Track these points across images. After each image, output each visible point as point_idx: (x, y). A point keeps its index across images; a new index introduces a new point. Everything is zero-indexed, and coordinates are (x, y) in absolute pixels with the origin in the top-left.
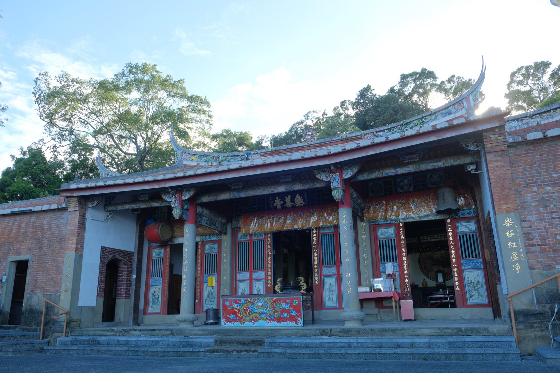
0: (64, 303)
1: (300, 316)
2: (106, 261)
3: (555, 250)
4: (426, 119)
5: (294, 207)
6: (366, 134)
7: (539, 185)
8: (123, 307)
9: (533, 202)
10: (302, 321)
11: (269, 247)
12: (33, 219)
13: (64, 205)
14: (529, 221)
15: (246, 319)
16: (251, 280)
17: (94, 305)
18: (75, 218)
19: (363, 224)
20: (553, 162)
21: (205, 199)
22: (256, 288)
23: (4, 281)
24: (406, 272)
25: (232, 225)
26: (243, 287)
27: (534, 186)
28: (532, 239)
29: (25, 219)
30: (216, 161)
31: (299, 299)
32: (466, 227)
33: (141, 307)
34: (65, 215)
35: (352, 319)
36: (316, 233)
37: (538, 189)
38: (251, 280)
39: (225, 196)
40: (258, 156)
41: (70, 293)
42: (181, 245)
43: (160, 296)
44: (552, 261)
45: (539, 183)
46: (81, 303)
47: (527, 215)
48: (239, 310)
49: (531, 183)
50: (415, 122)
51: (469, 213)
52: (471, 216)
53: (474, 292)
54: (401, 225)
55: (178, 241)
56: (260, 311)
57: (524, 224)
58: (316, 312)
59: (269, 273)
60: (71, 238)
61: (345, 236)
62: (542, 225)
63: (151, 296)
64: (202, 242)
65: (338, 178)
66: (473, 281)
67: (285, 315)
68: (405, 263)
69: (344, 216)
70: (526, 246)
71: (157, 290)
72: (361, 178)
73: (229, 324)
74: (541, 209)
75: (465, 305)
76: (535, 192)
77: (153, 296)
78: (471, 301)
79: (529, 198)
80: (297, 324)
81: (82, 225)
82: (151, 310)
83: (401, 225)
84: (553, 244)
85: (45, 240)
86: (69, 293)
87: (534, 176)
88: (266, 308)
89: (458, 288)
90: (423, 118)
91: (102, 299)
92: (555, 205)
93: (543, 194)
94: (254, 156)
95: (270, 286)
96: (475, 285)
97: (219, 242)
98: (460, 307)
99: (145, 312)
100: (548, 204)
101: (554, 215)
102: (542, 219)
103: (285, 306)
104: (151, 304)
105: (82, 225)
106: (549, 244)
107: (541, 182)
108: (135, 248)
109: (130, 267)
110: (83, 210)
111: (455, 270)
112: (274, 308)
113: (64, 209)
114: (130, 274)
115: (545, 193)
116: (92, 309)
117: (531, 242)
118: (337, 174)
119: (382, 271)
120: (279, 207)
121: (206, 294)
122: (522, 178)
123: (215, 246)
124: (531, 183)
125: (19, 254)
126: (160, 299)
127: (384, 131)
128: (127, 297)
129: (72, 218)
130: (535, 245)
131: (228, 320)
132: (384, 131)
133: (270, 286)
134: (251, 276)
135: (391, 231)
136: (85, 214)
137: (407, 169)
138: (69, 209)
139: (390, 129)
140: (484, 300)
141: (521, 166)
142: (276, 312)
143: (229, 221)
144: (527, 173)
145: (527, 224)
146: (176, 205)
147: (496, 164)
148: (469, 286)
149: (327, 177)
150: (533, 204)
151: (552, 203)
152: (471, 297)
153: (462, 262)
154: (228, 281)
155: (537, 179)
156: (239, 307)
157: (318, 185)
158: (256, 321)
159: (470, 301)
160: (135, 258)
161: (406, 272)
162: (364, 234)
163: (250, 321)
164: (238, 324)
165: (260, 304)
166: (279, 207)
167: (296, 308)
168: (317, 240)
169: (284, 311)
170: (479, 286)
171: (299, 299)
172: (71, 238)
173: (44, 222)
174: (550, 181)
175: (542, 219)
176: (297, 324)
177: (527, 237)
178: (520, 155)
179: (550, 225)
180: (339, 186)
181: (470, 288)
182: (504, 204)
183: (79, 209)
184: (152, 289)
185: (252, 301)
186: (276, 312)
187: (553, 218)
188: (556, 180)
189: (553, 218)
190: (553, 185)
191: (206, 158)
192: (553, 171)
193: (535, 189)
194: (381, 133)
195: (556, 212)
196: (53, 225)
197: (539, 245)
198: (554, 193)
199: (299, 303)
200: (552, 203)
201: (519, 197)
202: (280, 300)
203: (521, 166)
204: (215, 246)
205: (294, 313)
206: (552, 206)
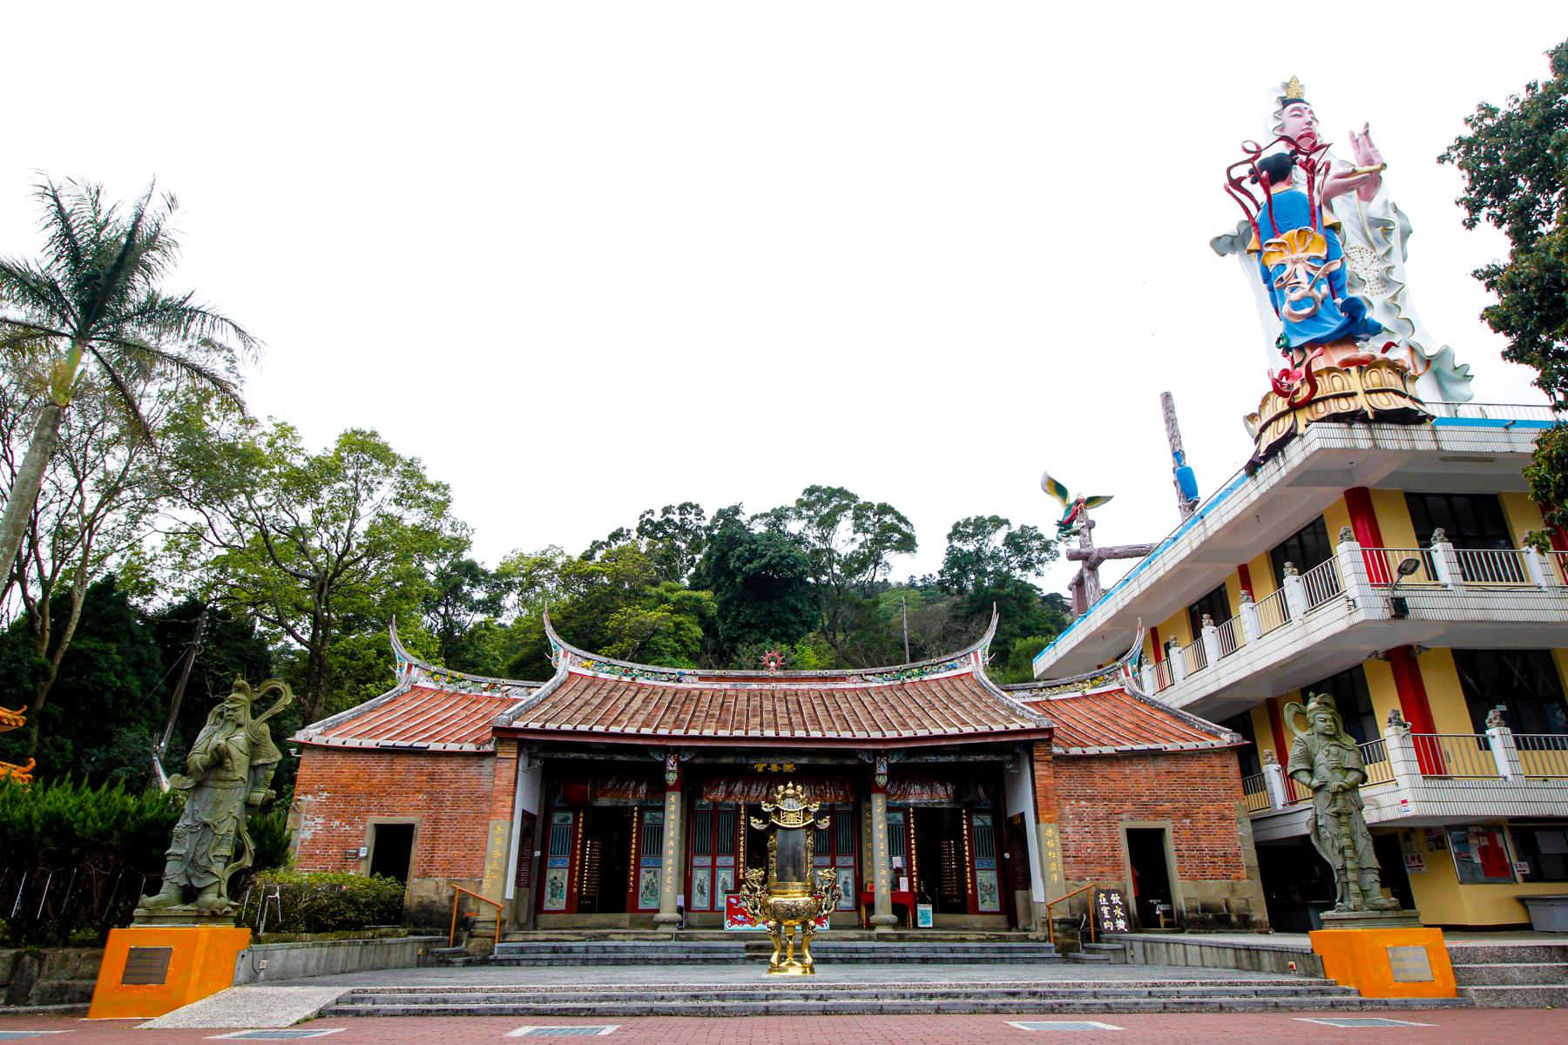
12: (426, 765)
13: (489, 748)
16: (713, 868)
23: (362, 855)
29: (402, 764)
35: (887, 924)
38: (713, 868)
40: (695, 679)
63: (548, 884)
73: (736, 927)
82: (548, 906)
94: (689, 679)
104: (548, 896)
121: (643, 884)
125: (393, 813)
131: (734, 921)
134: (714, 861)
140: (996, 907)
159: (982, 908)
164: (747, 926)
184: (551, 874)
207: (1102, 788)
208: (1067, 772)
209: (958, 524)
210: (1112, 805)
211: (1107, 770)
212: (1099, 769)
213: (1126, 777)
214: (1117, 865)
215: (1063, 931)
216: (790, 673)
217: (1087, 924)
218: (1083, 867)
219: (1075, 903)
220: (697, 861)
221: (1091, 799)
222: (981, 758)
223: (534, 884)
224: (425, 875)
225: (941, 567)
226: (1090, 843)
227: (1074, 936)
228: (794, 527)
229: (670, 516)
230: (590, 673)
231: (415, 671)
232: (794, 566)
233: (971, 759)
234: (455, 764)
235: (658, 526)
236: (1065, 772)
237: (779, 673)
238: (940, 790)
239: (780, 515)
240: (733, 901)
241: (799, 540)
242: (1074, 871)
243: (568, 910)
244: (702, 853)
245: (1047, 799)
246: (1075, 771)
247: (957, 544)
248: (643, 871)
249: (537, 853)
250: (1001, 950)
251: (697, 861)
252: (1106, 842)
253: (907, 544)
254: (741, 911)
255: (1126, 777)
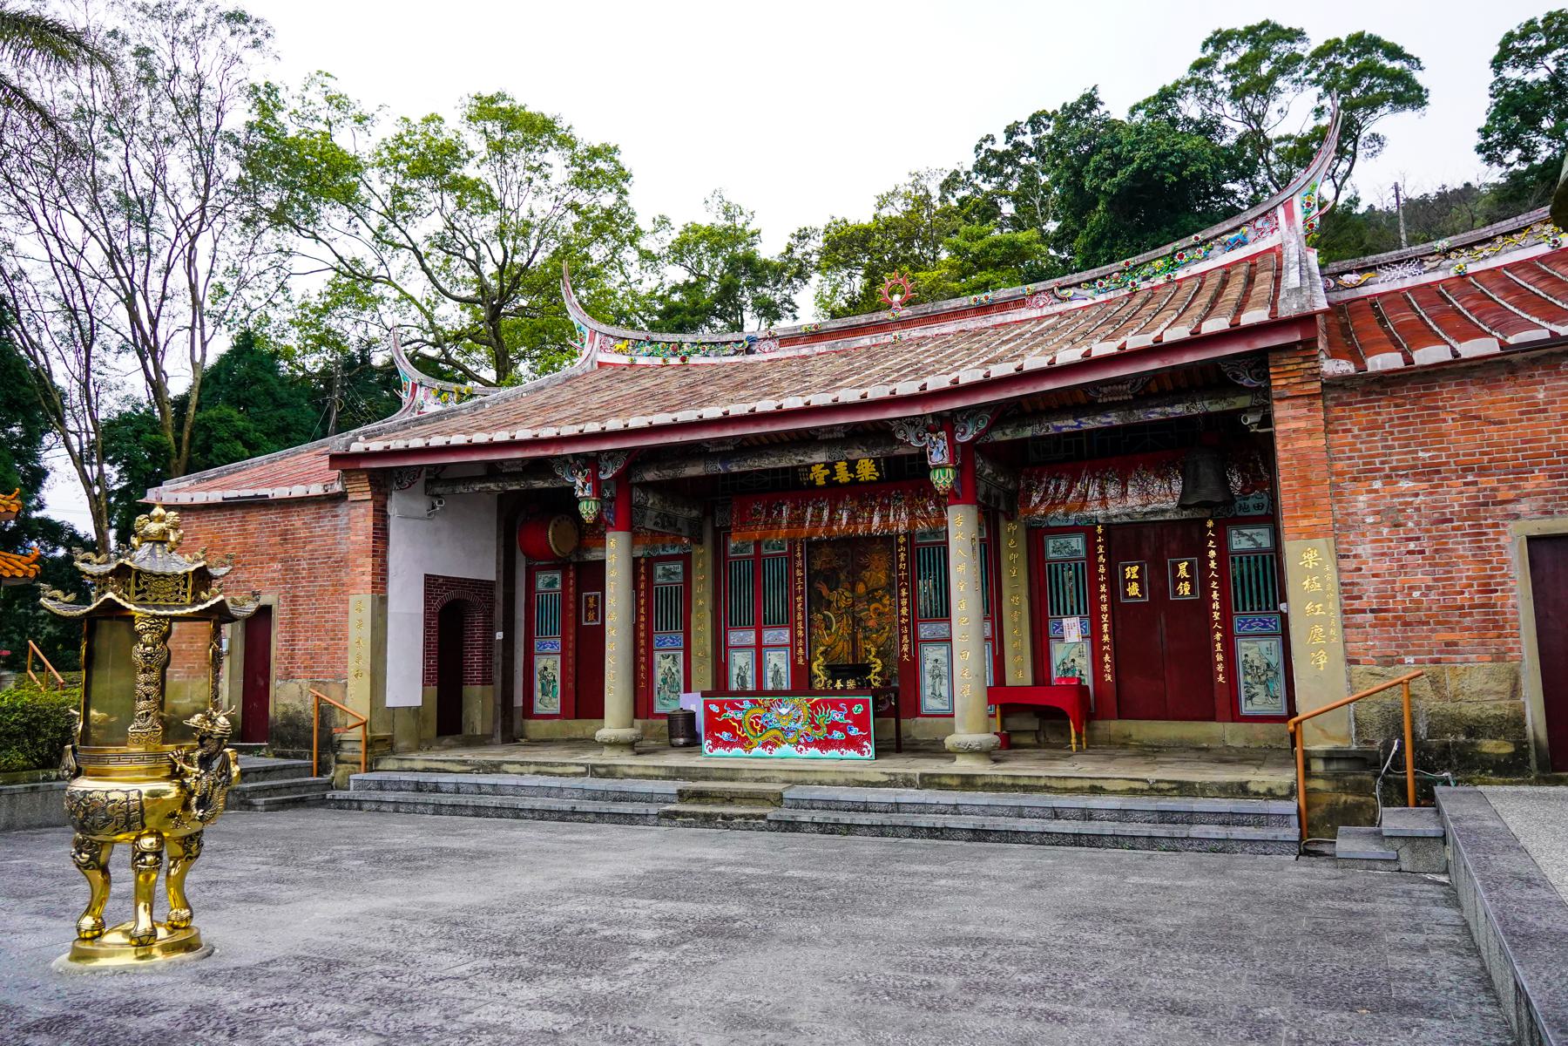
0: (356, 702)
1: (868, 738)
2: (436, 606)
3: (1406, 624)
4: (1181, 257)
5: (855, 481)
6: (1035, 293)
7: (1389, 476)
8: (479, 704)
9: (1369, 514)
10: (872, 749)
11: (799, 573)
13: (338, 488)
14: (1355, 556)
15: (756, 741)
16: (759, 648)
17: (417, 701)
18: (364, 516)
19: (1012, 527)
20: (1422, 423)
21: (650, 476)
22: (771, 665)
24: (1106, 638)
25: (713, 522)
26: (741, 662)
27: (1375, 479)
28: (1360, 598)
29: (256, 520)
30: (674, 356)
31: (865, 703)
32: (1250, 538)
33: (519, 701)
34: (342, 510)
35: (970, 751)
36: (905, 544)
37: (1384, 484)
38: (759, 648)
39: (692, 471)
41: (368, 680)
42: (601, 564)
43: (558, 678)
44: (1398, 646)
45: (1387, 471)
46: (390, 702)
47: (1353, 543)
48: (739, 722)
49: (1370, 471)
50: (1156, 264)
51: (1258, 507)
52: (1262, 512)
53: (1259, 689)
54: (1100, 530)
55: (593, 556)
56: (782, 724)
57: (1345, 564)
58: (905, 723)
59: (800, 633)
60: (359, 562)
61: (960, 569)
62: (1386, 564)
63: (537, 676)
64: (648, 559)
65: (942, 445)
66: (1257, 663)
67: (837, 735)
68: (1105, 618)
69: (961, 526)
70: (1345, 612)
71: (550, 663)
72: (998, 436)
73: (719, 751)
74: (1385, 531)
75: (1236, 716)
76: (1376, 491)
77: (544, 677)
78: (1249, 707)
79: (1361, 505)
80: (863, 753)
81: (381, 534)
82: (539, 708)
83: (1100, 530)
84: (1404, 610)
85: (304, 564)
86: (366, 680)
87: (1378, 455)
88: (797, 720)
89: (1221, 678)
90: (1174, 253)
91: (433, 689)
92: (1418, 524)
93: (1392, 497)
95: (801, 661)
96: (1261, 671)
97: (686, 559)
98: (1224, 720)
99: (528, 711)
100: (1401, 520)
101: (1412, 546)
102: (1383, 554)
103: (838, 717)
104: (538, 695)
105: (381, 534)
106: (1394, 610)
107: (1392, 469)
108: (498, 572)
109: (489, 615)
110: (380, 498)
111: (1218, 636)
112: (813, 720)
113: (340, 498)
114: (489, 631)
115: (1397, 496)
116: (414, 712)
117: (1357, 604)
118: (943, 434)
119: (1052, 635)
120: (820, 482)
121: (659, 675)
122: (1350, 458)
123: (678, 567)
124: (1370, 471)
126: (558, 683)
127: (1078, 285)
128: (487, 680)
129: (357, 521)
130: (1364, 611)
131: (717, 743)
132: (1078, 285)
133: (801, 661)
134: (759, 637)
135: (1077, 543)
136: (385, 506)
137: (1105, 420)
138: (351, 497)
139: (1094, 280)
141: (1349, 431)
142: (817, 728)
143: (708, 512)
144: (1363, 447)
145: (1350, 564)
146: (587, 493)
147: (1293, 425)
148: (1246, 674)
149: (919, 439)
150: (1370, 520)
151: (1410, 517)
152: (1251, 698)
153: (1236, 619)
154: (709, 649)
155: (1383, 463)
156: (739, 716)
157: (902, 451)
158: (775, 745)
159: (1247, 708)
160: (499, 595)
161: (1106, 638)
162: (1014, 551)
163: (764, 746)
164: (737, 751)
165: (784, 711)
166: (820, 482)
167: (860, 721)
168: (906, 561)
169: (834, 726)
170: (1271, 674)
171: (865, 703)
172: (359, 562)
173: (298, 524)
174: (1412, 467)
175: (1383, 554)
176: (863, 753)
177: (1349, 591)
178: (1350, 404)
179: (1402, 567)
180: (946, 460)
181: (1249, 678)
182: (1306, 517)
183: (373, 495)
184: (540, 663)
185: (767, 703)
186: (817, 728)
187: (1410, 552)
188: (1424, 466)
189: (1410, 552)
190: (1417, 476)
191: (650, 348)
192: (1421, 444)
193: (1377, 485)
194: (1070, 292)
195: (1418, 539)
196: (318, 531)
197: (1372, 611)
198: (1417, 495)
199: (866, 711)
200: (1410, 517)
201: (1339, 502)
202: (825, 703)
203: (1349, 431)
204: (678, 567)
205: (854, 732)
206: (1410, 524)
207: (1460, 443)
208: (1362, 416)
209: (1510, 36)
210: (1484, 482)
211: (1478, 398)
212: (1454, 400)
213: (1535, 410)
214: (1494, 623)
215: (1336, 776)
216: (928, 308)
217: (1398, 763)
218: (1397, 631)
219: (1371, 713)
220: (735, 637)
221: (1429, 472)
222: (1180, 409)
223: (498, 678)
224: (288, 676)
225: (1483, 123)
226: (1421, 578)
227: (1361, 788)
228: (1191, 107)
229: (1020, 138)
230: (625, 360)
231: (421, 393)
232: (1184, 165)
233: (1155, 415)
234: (308, 515)
235: (1003, 158)
236: (1356, 418)
237: (906, 312)
238: (1157, 486)
239: (1167, 96)
240: (715, 708)
241: (1209, 128)
242: (1375, 643)
243: (563, 715)
244: (741, 626)
245: (1306, 482)
246: (1386, 411)
247: (1511, 73)
248: (657, 656)
249: (499, 636)
250: (1165, 816)
251: (735, 637)
252: (1466, 571)
253: (1410, 95)
254: (726, 726)
255: (1535, 410)
